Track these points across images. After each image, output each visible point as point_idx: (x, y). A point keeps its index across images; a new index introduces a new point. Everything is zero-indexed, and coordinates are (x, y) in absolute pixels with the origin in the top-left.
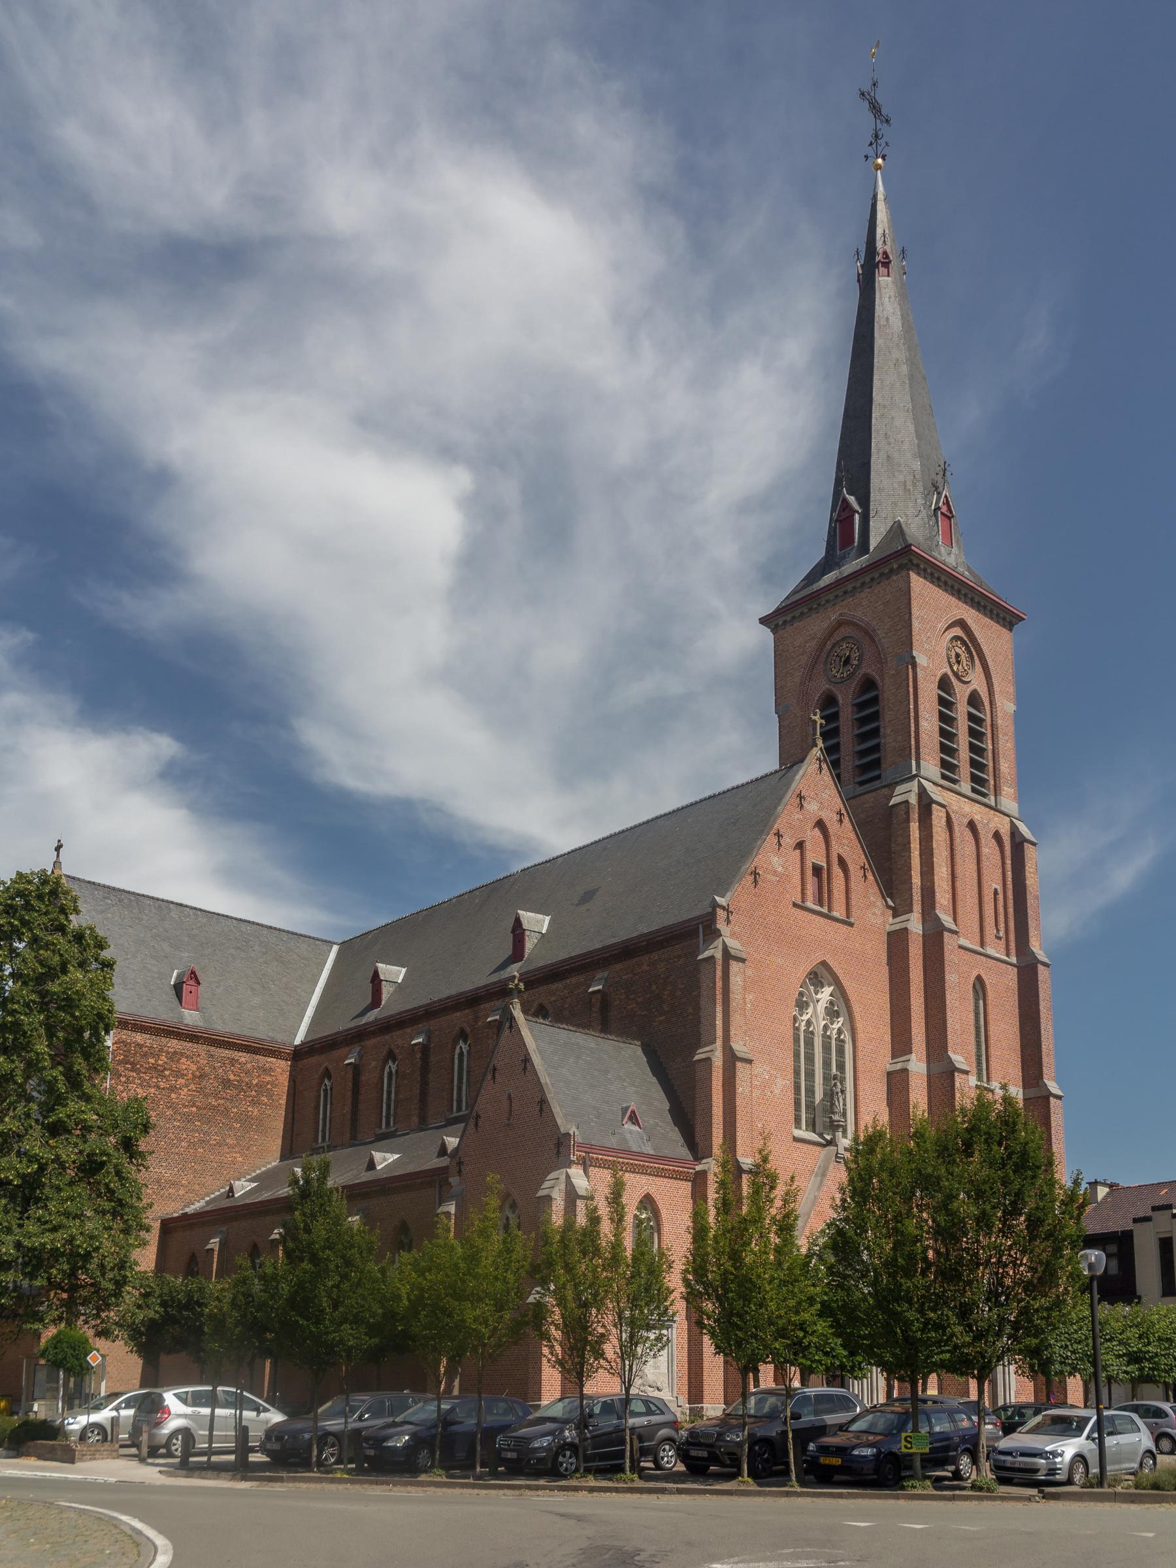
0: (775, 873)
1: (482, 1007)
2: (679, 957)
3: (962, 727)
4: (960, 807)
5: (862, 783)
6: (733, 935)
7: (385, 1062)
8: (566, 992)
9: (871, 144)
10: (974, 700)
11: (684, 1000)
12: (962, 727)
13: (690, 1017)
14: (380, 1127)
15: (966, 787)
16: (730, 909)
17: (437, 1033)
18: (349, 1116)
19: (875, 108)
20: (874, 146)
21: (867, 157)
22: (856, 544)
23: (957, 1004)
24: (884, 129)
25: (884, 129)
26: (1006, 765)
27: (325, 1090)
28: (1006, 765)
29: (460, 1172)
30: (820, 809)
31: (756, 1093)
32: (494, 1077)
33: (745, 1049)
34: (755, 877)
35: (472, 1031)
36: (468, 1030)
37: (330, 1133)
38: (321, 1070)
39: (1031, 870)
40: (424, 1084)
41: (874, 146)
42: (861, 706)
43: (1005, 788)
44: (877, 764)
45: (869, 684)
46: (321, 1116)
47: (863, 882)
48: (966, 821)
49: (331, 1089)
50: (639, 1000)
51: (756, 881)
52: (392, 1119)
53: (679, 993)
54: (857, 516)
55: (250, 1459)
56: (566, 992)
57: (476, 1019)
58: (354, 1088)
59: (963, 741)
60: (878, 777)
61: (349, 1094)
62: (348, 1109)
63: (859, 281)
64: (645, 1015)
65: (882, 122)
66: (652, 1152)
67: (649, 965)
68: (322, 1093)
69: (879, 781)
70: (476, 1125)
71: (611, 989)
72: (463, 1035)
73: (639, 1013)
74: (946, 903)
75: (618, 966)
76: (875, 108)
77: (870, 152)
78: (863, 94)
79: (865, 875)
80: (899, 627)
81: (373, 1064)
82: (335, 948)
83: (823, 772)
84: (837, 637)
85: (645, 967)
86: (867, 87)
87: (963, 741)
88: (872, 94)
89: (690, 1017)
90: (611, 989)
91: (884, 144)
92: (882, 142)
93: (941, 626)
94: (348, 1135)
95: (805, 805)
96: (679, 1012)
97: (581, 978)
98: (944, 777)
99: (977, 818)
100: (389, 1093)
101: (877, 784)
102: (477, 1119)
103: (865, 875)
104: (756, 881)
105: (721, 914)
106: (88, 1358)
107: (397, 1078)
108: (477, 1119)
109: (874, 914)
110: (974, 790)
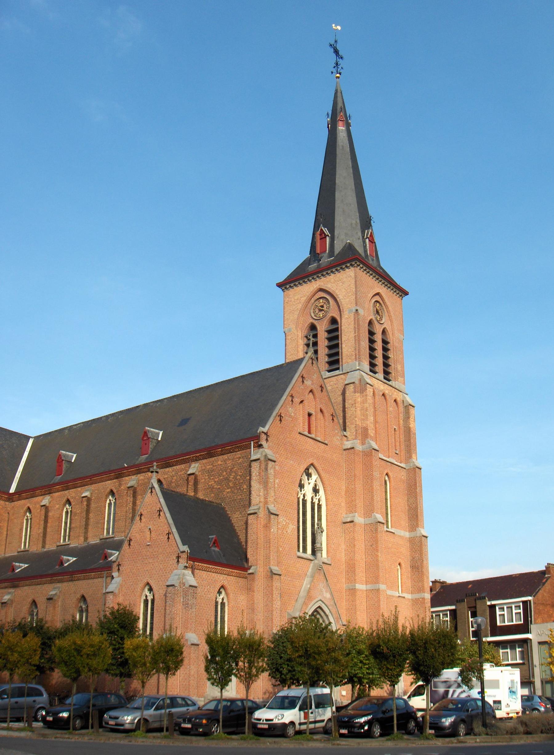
0: (290, 416)
1: (124, 478)
2: (240, 458)
3: (379, 346)
4: (379, 387)
5: (329, 371)
6: (269, 447)
7: (65, 505)
8: (173, 473)
9: (334, 67)
10: (384, 332)
11: (242, 481)
12: (379, 346)
13: (245, 490)
14: (60, 542)
15: (381, 376)
16: (268, 434)
17: (96, 491)
18: (42, 535)
19: (336, 52)
20: (336, 68)
21: (332, 72)
22: (327, 251)
23: (379, 488)
24: (340, 61)
25: (340, 61)
26: (400, 366)
27: (27, 520)
28: (400, 366)
29: (119, 569)
30: (312, 384)
31: (280, 531)
32: (141, 519)
33: (275, 509)
34: (280, 418)
35: (117, 492)
36: (115, 491)
37: (29, 543)
38: (25, 508)
39: (412, 420)
40: (87, 519)
41: (336, 68)
42: (329, 332)
43: (400, 378)
44: (337, 362)
45: (334, 321)
46: (24, 534)
47: (332, 423)
48: (381, 393)
49: (31, 519)
50: (216, 480)
51: (281, 420)
52: (67, 537)
53: (238, 477)
54: (328, 239)
55: (33, 726)
56: (173, 473)
57: (120, 485)
58: (45, 519)
59: (379, 353)
60: (338, 369)
61: (42, 522)
62: (41, 530)
63: (328, 127)
64: (219, 488)
65: (339, 58)
66: (225, 562)
67: (222, 462)
68: (25, 521)
69: (338, 371)
70: (130, 544)
71: (200, 473)
72: (112, 493)
73: (216, 487)
74: (373, 435)
75: (204, 461)
76: (336, 52)
77: (334, 70)
78: (331, 45)
79: (333, 419)
80: (350, 294)
81: (57, 506)
82: (31, 442)
83: (313, 365)
84: (317, 296)
85: (220, 462)
86: (332, 43)
87: (379, 353)
88: (335, 45)
89: (245, 490)
90: (200, 473)
91: (340, 68)
92: (340, 67)
93: (371, 295)
94: (41, 545)
95: (305, 382)
96: (238, 487)
97: (183, 466)
98: (371, 371)
99: (387, 392)
100: (66, 523)
101: (337, 372)
102: (130, 541)
103: (333, 419)
104: (281, 420)
105: (263, 437)
106: (522, 622)
107: (71, 514)
108: (130, 541)
109: (337, 439)
110: (385, 378)
